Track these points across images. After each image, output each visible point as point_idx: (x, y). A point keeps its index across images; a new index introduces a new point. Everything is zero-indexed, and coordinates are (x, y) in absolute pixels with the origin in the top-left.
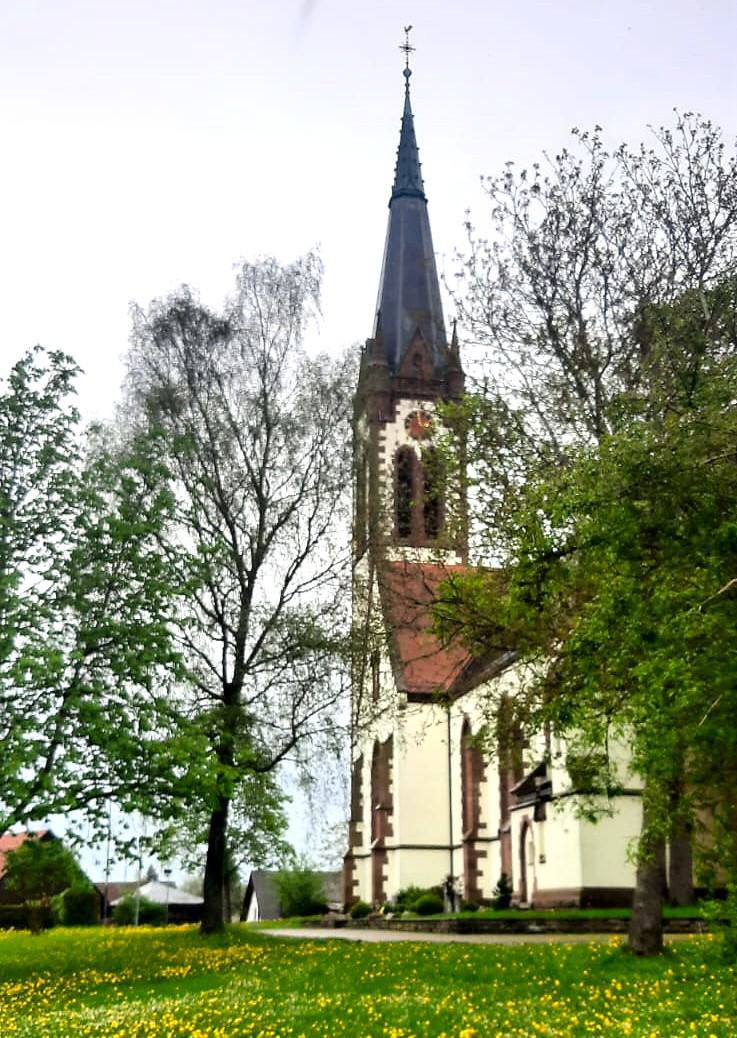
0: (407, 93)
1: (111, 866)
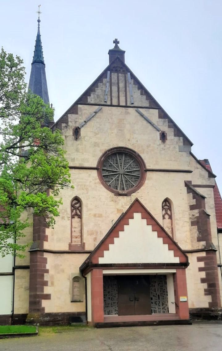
0: (39, 28)
1: (27, 247)
